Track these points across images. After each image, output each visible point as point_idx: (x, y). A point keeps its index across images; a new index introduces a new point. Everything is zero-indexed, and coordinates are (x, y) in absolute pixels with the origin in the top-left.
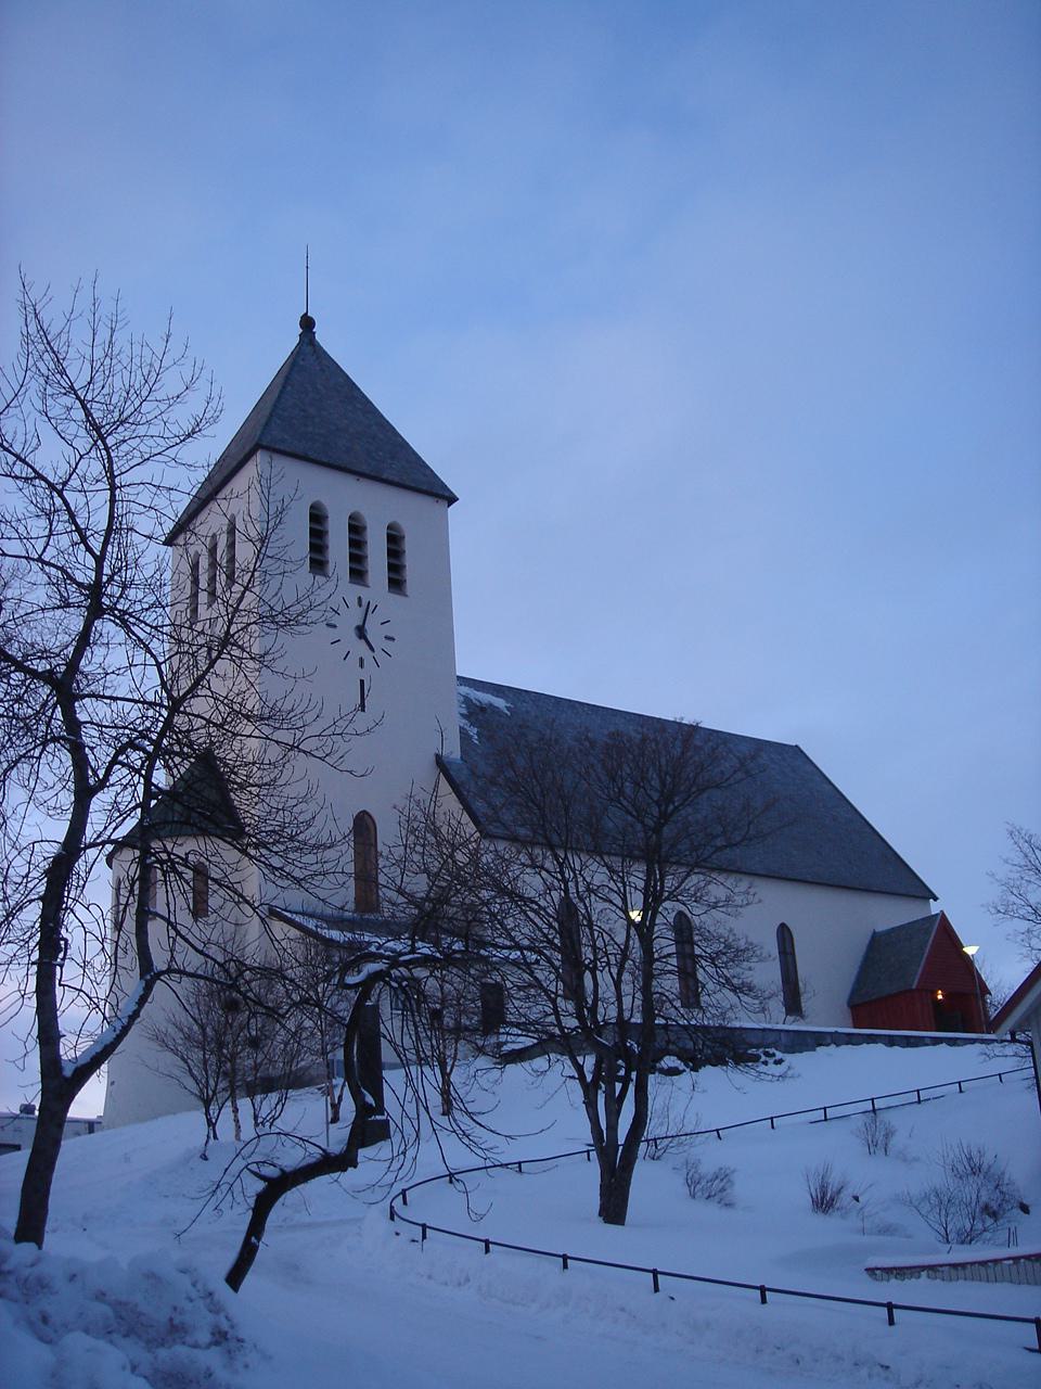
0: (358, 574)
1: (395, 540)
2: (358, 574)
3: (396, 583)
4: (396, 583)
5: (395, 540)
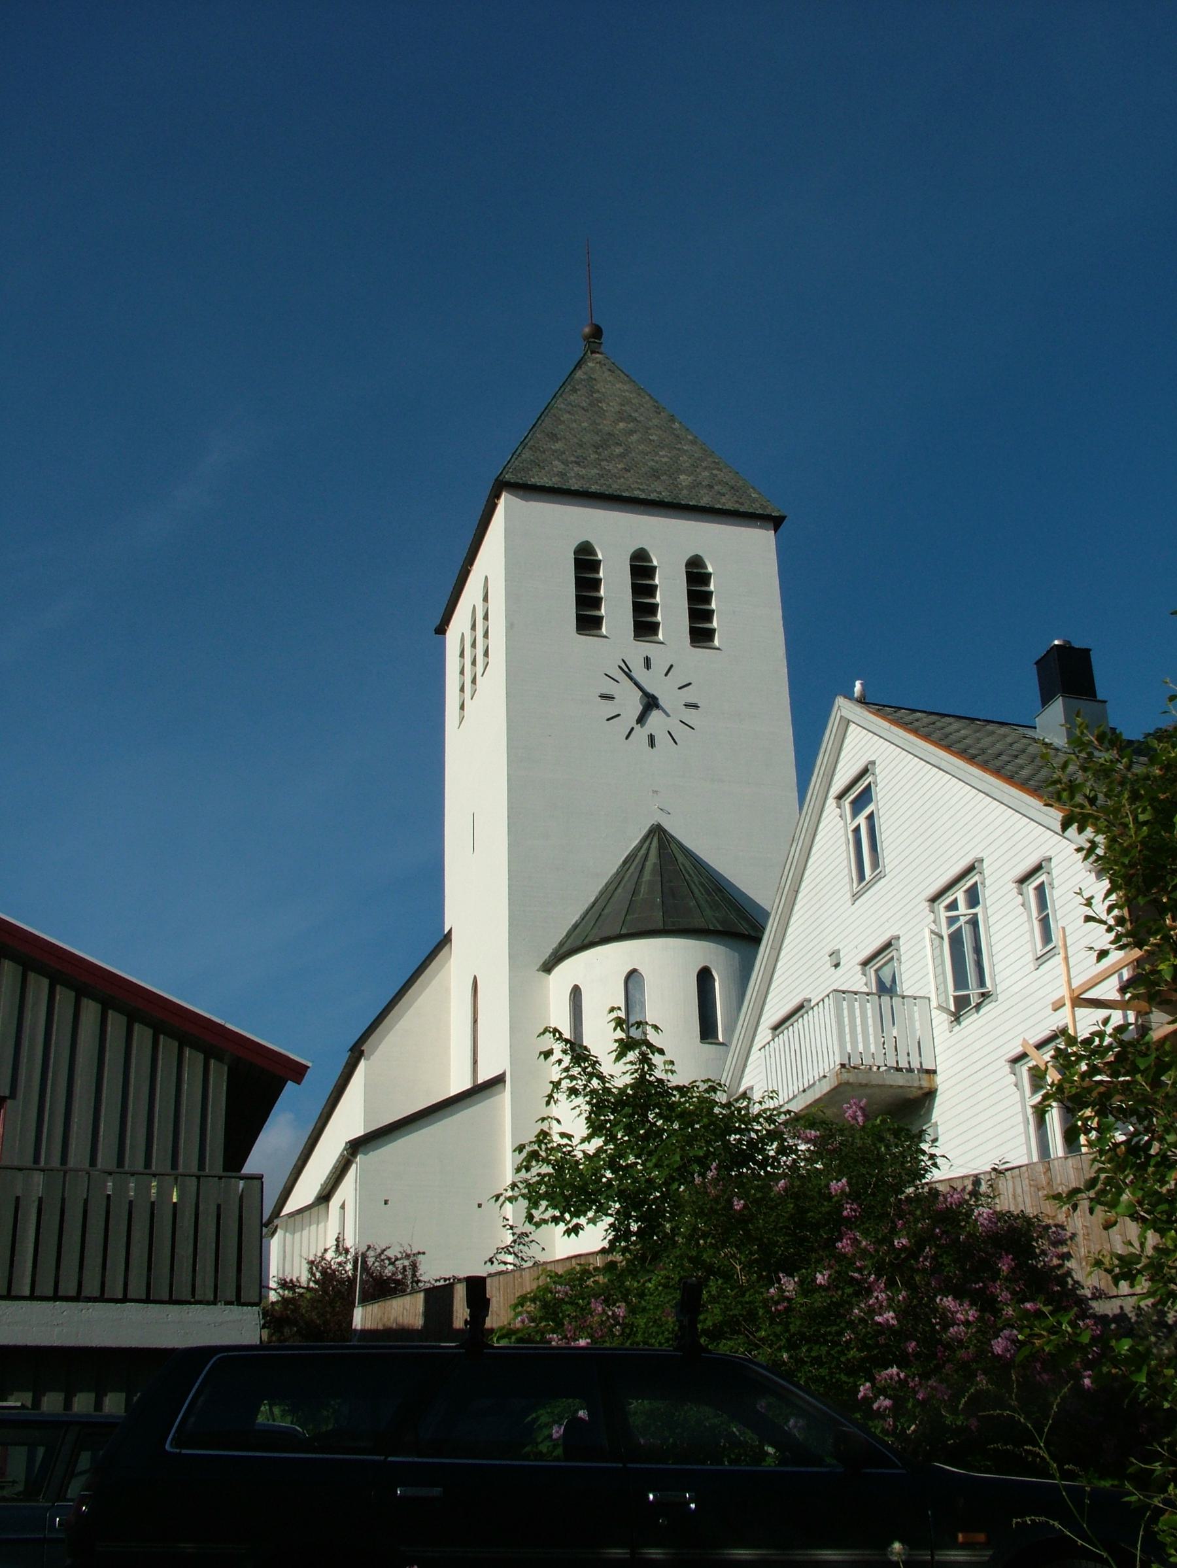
0: (645, 627)
1: (697, 575)
2: (645, 627)
3: (701, 635)
4: (701, 635)
5: (697, 575)
